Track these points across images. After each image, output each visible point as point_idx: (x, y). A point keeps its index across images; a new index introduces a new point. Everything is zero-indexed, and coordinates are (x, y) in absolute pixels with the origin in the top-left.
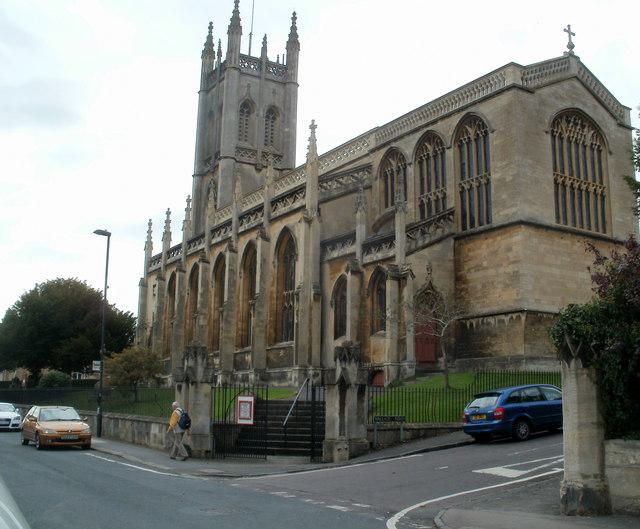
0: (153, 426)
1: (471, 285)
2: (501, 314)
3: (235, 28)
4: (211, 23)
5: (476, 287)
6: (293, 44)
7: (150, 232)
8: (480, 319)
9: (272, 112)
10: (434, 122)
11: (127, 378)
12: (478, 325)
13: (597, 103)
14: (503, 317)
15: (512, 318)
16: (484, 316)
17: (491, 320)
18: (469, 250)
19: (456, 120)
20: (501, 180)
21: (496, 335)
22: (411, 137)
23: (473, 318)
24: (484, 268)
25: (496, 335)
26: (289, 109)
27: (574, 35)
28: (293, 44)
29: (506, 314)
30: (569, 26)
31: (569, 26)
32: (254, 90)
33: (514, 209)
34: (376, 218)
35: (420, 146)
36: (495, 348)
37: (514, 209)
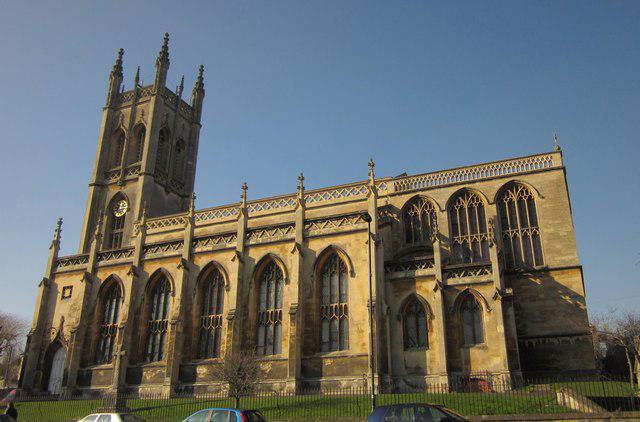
6: (200, 90)
7: (59, 231)
8: (541, 340)
9: (180, 145)
10: (473, 182)
11: (501, 292)
13: (281, 246)
16: (545, 337)
17: (555, 341)
19: (498, 184)
20: (554, 237)
22: (501, 180)
23: (532, 337)
24: (540, 299)
27: (370, 165)
28: (200, 90)
29: (571, 335)
32: (171, 120)
33: (571, 257)
34: (399, 251)
37: (571, 257)
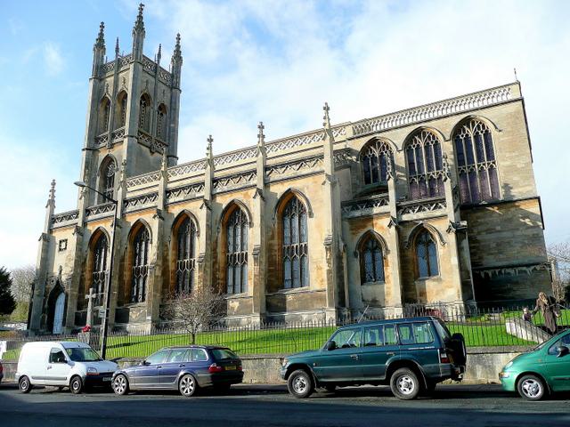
0: (395, 341)
1: (482, 244)
2: (523, 266)
3: (139, 29)
4: (103, 23)
5: (489, 245)
6: (178, 58)
8: (497, 271)
12: (494, 274)
14: (524, 268)
15: (535, 269)
18: (478, 218)
21: (517, 283)
23: (489, 268)
25: (517, 283)
26: (175, 109)
28: (178, 58)
29: (528, 266)
30: (326, 104)
31: (326, 104)
35: (410, 139)
36: (518, 293)
